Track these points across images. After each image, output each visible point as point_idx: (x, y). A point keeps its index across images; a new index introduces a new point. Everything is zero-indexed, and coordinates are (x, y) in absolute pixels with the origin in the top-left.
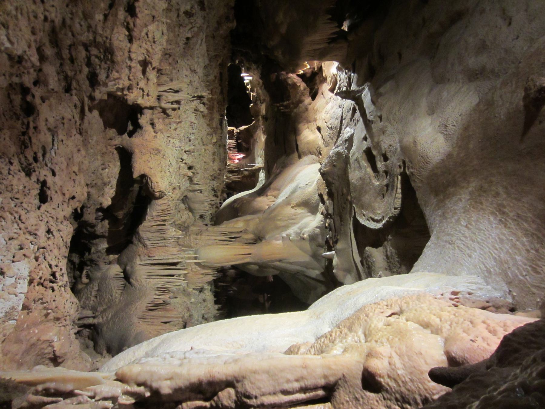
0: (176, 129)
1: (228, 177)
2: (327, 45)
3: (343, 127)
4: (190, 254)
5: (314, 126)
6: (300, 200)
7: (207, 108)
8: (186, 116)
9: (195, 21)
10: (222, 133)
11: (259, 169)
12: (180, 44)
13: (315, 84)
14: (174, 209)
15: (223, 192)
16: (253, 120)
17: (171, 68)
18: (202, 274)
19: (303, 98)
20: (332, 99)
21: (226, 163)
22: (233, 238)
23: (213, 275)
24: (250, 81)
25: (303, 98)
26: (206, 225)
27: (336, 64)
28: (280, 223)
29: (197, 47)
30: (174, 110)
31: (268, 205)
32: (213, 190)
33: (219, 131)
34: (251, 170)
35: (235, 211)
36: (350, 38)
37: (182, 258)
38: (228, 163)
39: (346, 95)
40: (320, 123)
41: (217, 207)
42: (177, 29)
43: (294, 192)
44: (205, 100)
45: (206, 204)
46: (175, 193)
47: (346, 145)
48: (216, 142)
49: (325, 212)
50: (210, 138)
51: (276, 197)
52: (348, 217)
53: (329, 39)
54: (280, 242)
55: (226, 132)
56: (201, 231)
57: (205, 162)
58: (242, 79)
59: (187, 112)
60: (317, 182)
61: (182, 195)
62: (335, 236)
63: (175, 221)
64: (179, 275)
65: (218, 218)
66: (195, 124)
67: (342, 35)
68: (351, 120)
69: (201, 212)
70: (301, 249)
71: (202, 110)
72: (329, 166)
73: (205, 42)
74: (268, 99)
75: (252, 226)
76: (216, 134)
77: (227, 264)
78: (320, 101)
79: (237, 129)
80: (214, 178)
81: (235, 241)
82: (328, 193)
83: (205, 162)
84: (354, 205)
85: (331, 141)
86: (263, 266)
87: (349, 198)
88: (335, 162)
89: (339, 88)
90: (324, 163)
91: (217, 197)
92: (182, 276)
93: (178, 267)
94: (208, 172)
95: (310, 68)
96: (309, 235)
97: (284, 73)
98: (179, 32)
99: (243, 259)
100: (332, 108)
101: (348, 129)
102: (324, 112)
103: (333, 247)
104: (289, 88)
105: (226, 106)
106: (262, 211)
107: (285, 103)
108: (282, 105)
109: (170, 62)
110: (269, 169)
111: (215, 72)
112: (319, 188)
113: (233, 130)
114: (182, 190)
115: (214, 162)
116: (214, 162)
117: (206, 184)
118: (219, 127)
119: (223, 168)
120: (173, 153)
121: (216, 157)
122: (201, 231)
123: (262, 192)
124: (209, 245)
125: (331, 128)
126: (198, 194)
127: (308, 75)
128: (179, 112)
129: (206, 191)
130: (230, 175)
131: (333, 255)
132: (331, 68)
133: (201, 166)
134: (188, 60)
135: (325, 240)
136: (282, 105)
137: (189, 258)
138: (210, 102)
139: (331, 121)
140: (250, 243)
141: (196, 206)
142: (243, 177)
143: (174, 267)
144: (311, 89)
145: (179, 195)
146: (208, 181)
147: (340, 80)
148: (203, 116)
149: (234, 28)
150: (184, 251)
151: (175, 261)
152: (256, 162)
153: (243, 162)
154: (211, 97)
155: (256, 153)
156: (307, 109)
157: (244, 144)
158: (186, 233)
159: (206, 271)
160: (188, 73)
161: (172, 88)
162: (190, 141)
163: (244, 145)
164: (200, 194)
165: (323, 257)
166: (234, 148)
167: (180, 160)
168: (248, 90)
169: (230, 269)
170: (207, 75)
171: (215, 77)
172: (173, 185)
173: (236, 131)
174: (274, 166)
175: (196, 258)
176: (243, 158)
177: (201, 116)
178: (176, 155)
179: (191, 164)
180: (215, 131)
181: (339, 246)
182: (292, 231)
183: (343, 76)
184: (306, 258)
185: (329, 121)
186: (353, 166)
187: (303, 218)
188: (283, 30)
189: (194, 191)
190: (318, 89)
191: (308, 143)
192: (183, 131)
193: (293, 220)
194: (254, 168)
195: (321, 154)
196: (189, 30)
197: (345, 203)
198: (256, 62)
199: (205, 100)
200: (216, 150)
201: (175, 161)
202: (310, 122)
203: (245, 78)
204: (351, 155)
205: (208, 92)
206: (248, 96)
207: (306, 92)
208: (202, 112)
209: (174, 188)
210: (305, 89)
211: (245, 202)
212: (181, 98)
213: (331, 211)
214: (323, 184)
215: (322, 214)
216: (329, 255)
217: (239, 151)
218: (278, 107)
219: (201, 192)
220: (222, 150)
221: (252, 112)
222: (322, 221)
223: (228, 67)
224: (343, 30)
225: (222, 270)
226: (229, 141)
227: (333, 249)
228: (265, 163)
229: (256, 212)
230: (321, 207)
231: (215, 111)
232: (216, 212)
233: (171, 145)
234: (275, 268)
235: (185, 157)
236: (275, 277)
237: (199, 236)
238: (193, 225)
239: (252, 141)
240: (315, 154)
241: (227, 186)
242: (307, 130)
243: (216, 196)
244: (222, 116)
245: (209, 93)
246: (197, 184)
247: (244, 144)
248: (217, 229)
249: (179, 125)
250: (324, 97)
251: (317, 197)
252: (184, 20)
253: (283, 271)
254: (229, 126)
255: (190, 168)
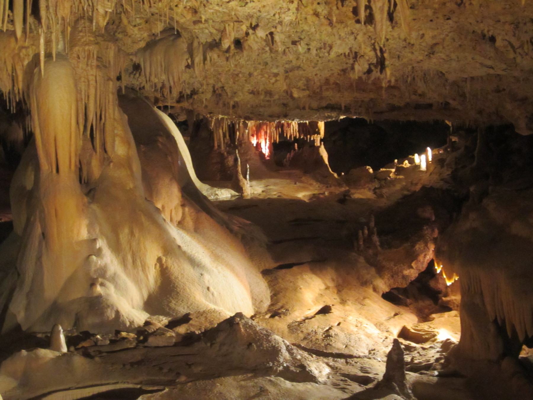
0: (316, 14)
1: (219, 121)
2: (491, 318)
3: (331, 361)
4: (57, 44)
5: (331, 299)
6: (176, 274)
7: (360, 78)
8: (343, 35)
9: (527, 54)
10: (311, 109)
11: (238, 188)
12: (482, 25)
13: (416, 299)
14: (153, 10)
15: (190, 112)
16: (339, 175)
17: (436, 6)
18: (14, 69)
19: (387, 276)
20: (386, 334)
21: (249, 119)
22: (92, 133)
23: (12, 92)
24: (419, 166)
25: (387, 276)
26: (119, 78)
27: (455, 338)
28: (124, 235)
29: (479, 59)
30: (355, 11)
31: (163, 207)
32: (194, 92)
33: (315, 104)
34: (237, 172)
35: (149, 140)
36: (506, 363)
37: (48, 28)
38: (250, 124)
39: (396, 360)
40: (337, 312)
41: (157, 101)
42: (509, 18)
43: (193, 262)
44: (376, 74)
45: (164, 77)
46: (185, 13)
47: (292, 368)
48: (292, 96)
49: (152, 329)
50: (301, 84)
51: (181, 224)
52: (140, 379)
53: (504, 321)
54: (84, 234)
55: (314, 118)
56: (105, 67)
57: (250, 75)
58: (421, 151)
59: (352, 37)
60: (214, 311)
61: (183, 28)
62: (100, 352)
63: (126, 12)
64: (12, 22)
65: (135, 104)
66: (329, 53)
67: (510, 347)
68: (344, 375)
69: (147, 68)
70: (71, 280)
71: (357, 67)
72: (249, 335)
73: (489, 74)
74: (384, 203)
75: (118, 174)
76: (309, 96)
77: (37, 122)
78: (381, 309)
79: (321, 140)
80: (218, 94)
81: (84, 140)
82: (193, 333)
83: (250, 75)
84: (167, 390)
85: (302, 336)
86: (32, 199)
87: (183, 379)
88: (258, 347)
89: (409, 349)
90: (254, 323)
91: (178, 101)
92: (11, 27)
93: (30, 19)
94: (231, 82)
95: (447, 287)
96: (100, 296)
97: (436, 234)
98: (505, 23)
99: (47, 155)
100: (369, 336)
101: (327, 370)
102: (360, 319)
103: (77, 349)
104: (407, 245)
105: (366, 118)
106: (151, 196)
107: (375, 238)
108: (371, 233)
109: (448, 5)
110: (240, 208)
111: (433, 95)
112: (201, 314)
113: (319, 133)
114: (191, 27)
115: (252, 92)
116: (252, 92)
117: (206, 77)
118: (324, 104)
119: (240, 112)
120: (267, 8)
121: (262, 97)
122: (105, 67)
123: (190, 195)
124: (76, 85)
125: (327, 335)
126: (185, 60)
127: (432, 284)
128: (351, 22)
129: (191, 77)
130: (225, 126)
131: (58, 348)
132: (447, 330)
133: (242, 66)
134: (454, 40)
135: (91, 332)
136: (371, 233)
137: (48, 42)
138: (374, 83)
139: (342, 335)
140: (81, 169)
141: (159, 57)
142: (222, 155)
143: (29, 11)
144: (405, 291)
145: (182, 21)
146: (211, 81)
147: (424, 349)
148: (344, 71)
149: (517, 131)
150: (63, 32)
151: (43, 13)
152: (254, 183)
153: (252, 153)
154: (384, 85)
155: (273, 180)
156: (365, 283)
157: (289, 156)
158: (102, 36)
159: (20, 78)
160: (428, 40)
161: (399, 7)
162: (294, 43)
163: (289, 157)
164: (184, 63)
165: (55, 326)
166: (281, 135)
167: (254, 24)
168: (399, 162)
169: (24, 130)
170: (425, 76)
171: (422, 95)
172: (202, 9)
173: (317, 139)
174: (248, 219)
175: (48, 56)
176: (262, 155)
177: (345, 66)
178: (264, 14)
179: (246, 45)
180: (315, 94)
181: (79, 360)
182: (109, 260)
183: (432, 353)
184: (51, 290)
185: (342, 330)
186: (250, 384)
187: (137, 282)
188: (517, 229)
189: (191, 53)
190: (406, 305)
191: (296, 289)
192: (313, 30)
193: (132, 260)
194: (241, 177)
195: (272, 316)
196: (510, 43)
197: (170, 370)
198: (454, 176)
199: (376, 74)
200: (276, 97)
201: (251, 11)
202: (339, 291)
203: (423, 157)
204: (273, 378)
205: (393, 80)
206: (388, 163)
207: (400, 280)
208: (353, 68)
209: (195, 11)
210: (404, 277)
211: (170, 159)
212: (379, 27)
213: (152, 341)
214: (211, 323)
215: (147, 323)
216: (59, 339)
217: (275, 147)
218: (367, 224)
219: (188, 66)
220: (277, 109)
221: (356, 172)
222: (132, 323)
223: (443, 121)
224: (520, 349)
225: (22, 112)
226: (295, 124)
227: (72, 349)
228: (252, 200)
229: (150, 184)
230: (162, 321)
231: (356, 95)
232: (147, 98)
233: (285, 5)
234: (29, 224)
235: (261, 33)
236: (9, 226)
237: (95, 63)
238: (119, 50)
239: (297, 172)
240: (272, 305)
241: (202, 120)
242: (323, 287)
243: (181, 98)
244: (347, 110)
245: (390, 81)
246: (205, 59)
247: (289, 156)
248: (111, 99)
249: (326, 22)
250: (390, 318)
251: (182, 310)
252: (526, 32)
253: (22, 244)
254: (326, 124)
255: (238, 43)
